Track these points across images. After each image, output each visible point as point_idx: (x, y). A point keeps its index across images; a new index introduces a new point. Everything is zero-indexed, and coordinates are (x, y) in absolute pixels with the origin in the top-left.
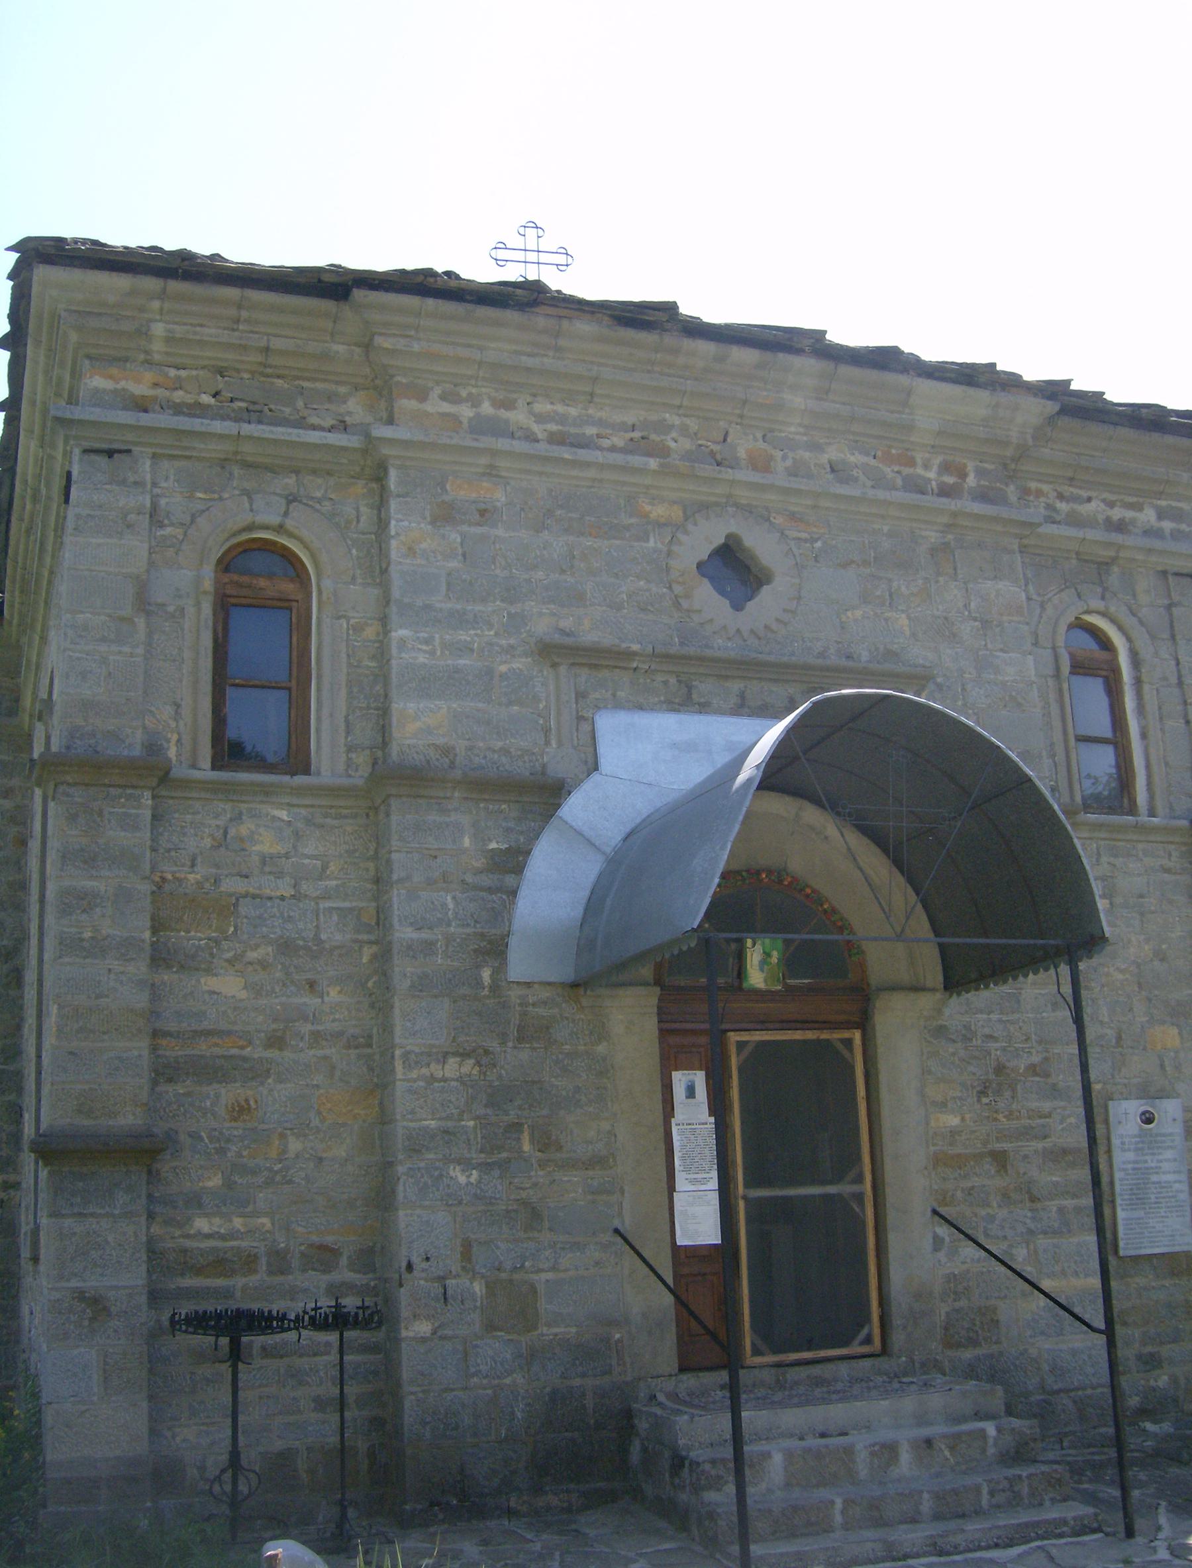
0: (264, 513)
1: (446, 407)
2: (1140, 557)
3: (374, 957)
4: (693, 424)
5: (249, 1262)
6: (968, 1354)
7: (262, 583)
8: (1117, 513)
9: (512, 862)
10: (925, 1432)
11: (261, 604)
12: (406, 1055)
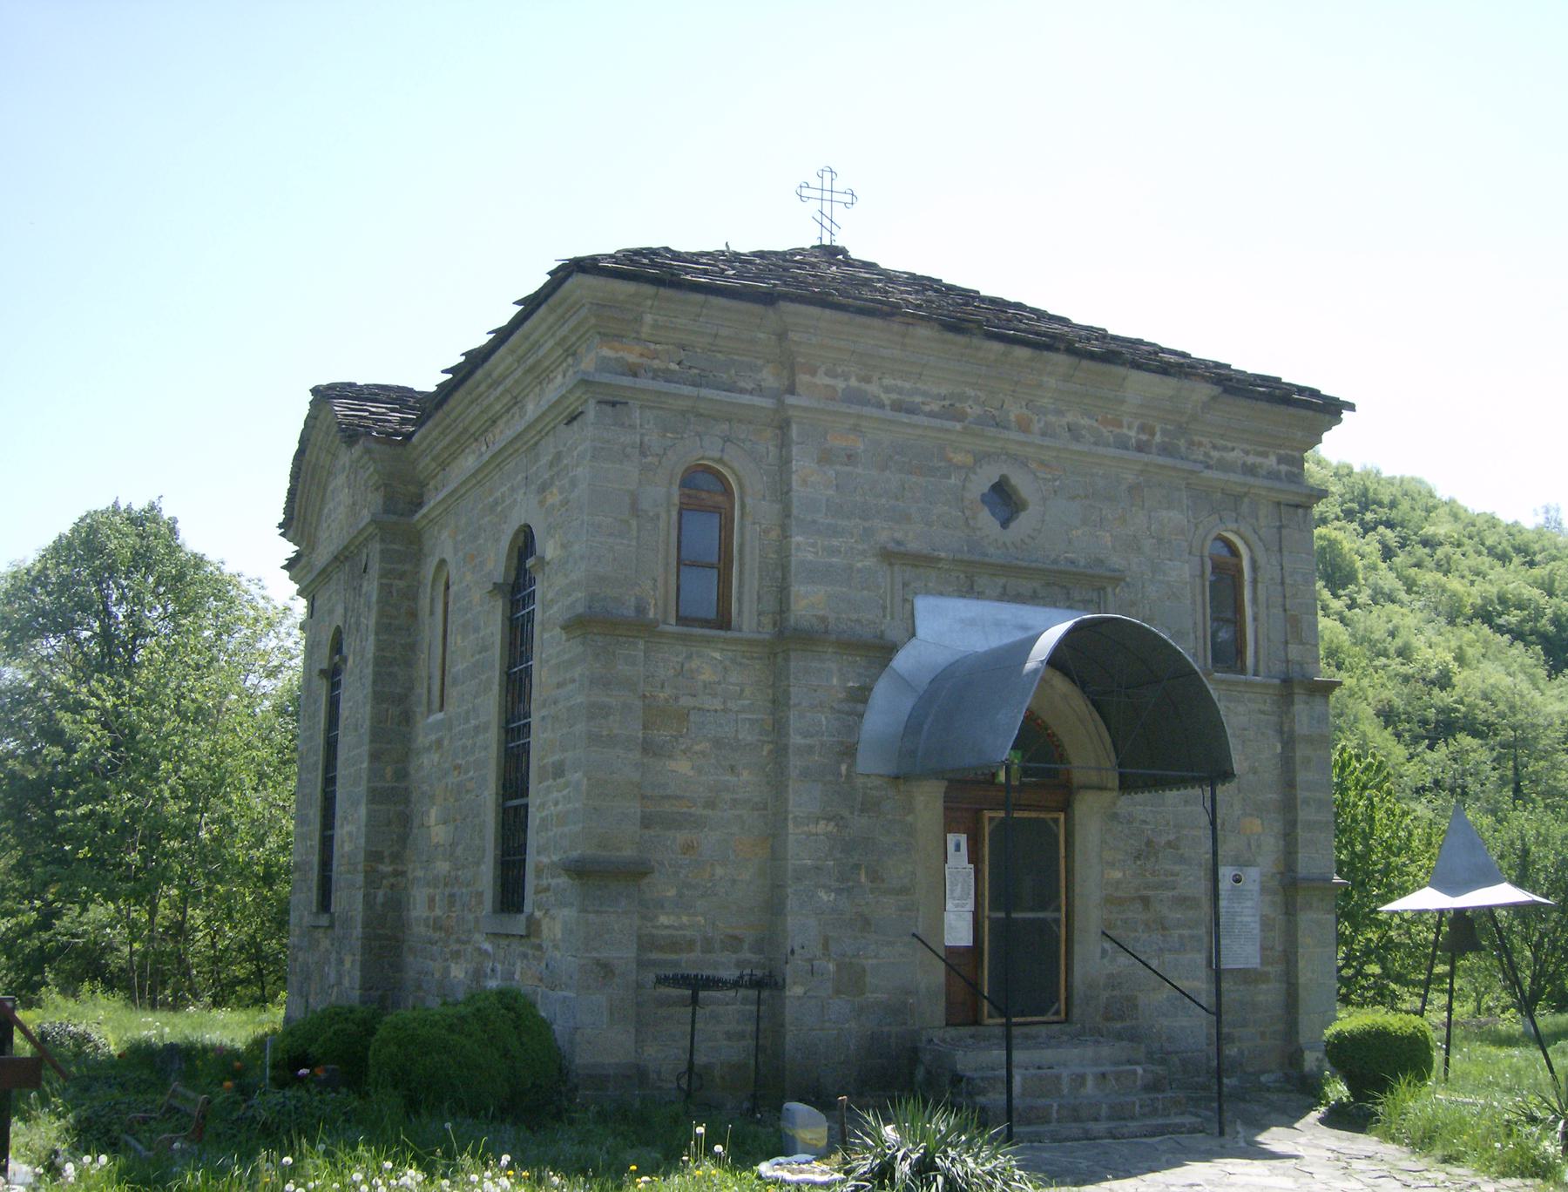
0: (707, 450)
1: (828, 381)
2: (1264, 493)
3: (770, 752)
4: (982, 396)
5: (690, 945)
6: (1119, 1025)
7: (704, 495)
8: (1251, 459)
9: (861, 695)
10: (1102, 1069)
11: (702, 509)
12: (795, 818)
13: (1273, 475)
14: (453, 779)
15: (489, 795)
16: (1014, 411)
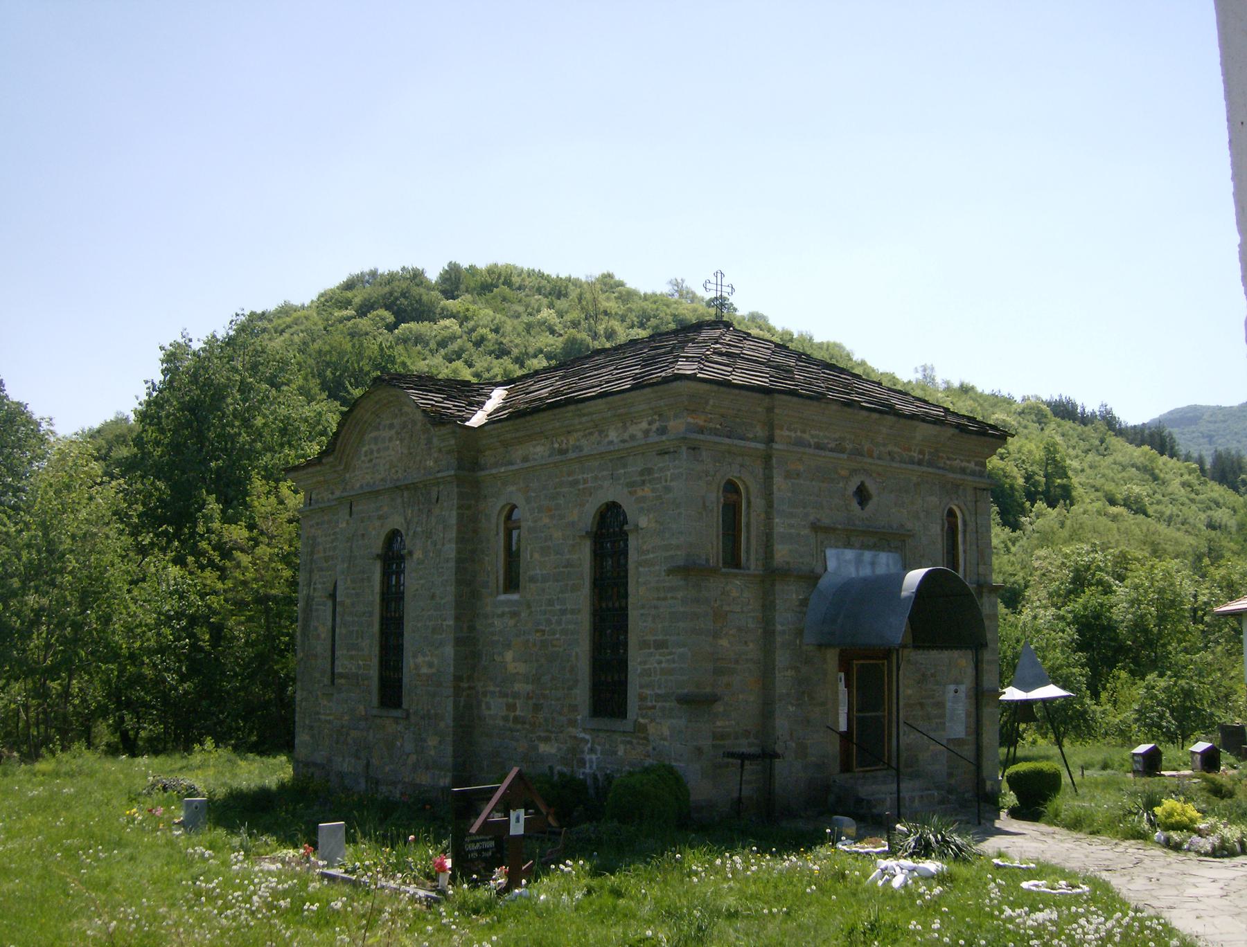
0: (733, 473)
1: (787, 433)
13: (973, 473)
16: (867, 446)
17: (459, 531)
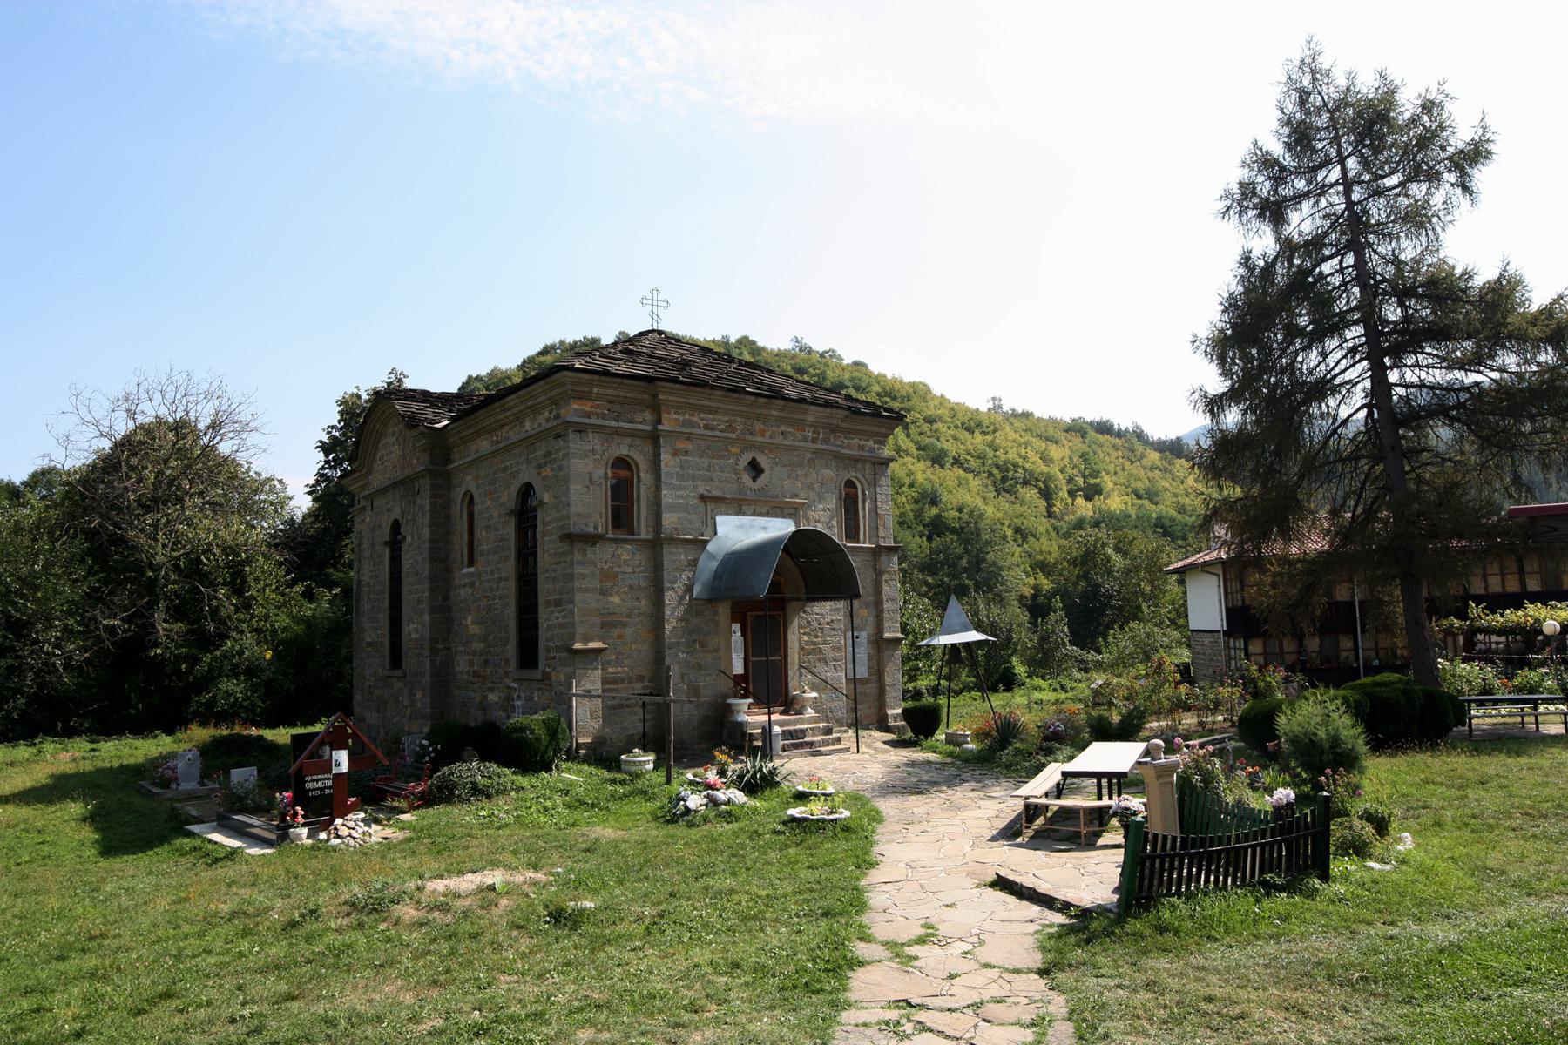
5: (622, 680)
14: (484, 603)
15: (511, 612)
17: (432, 517)
